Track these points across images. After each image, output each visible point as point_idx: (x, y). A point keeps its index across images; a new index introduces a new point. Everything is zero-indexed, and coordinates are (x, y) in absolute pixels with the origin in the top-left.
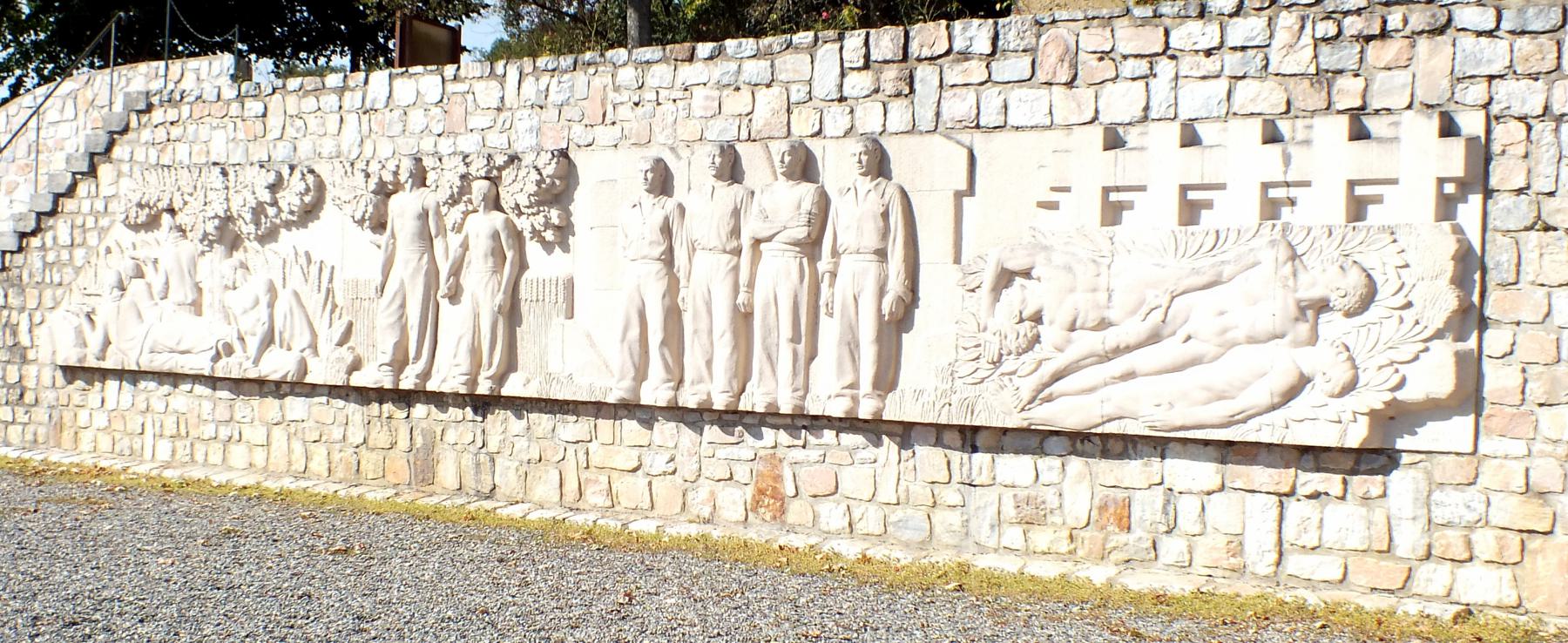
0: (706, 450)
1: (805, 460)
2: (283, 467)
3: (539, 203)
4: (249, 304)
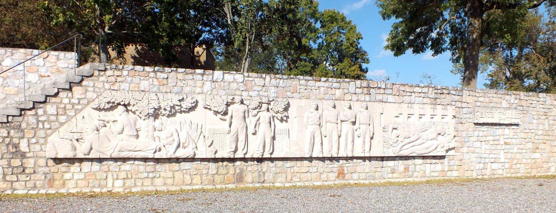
0: (325, 166)
1: (348, 166)
2: (181, 182)
4: (169, 135)
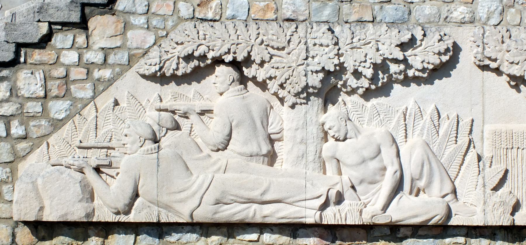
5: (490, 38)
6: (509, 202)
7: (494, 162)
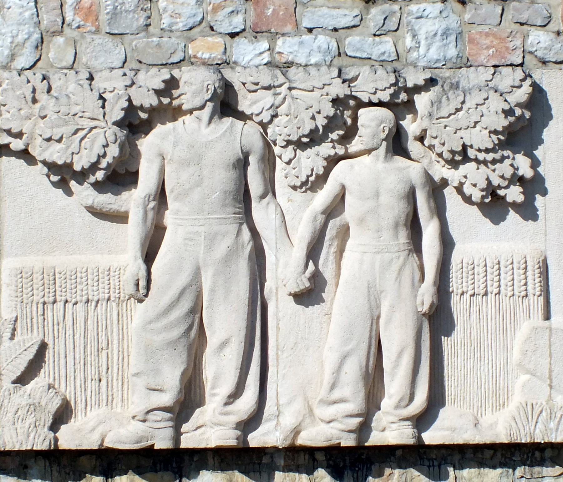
3: (501, 145)
5: (10, 93)
6: (46, 404)
7: (19, 330)
